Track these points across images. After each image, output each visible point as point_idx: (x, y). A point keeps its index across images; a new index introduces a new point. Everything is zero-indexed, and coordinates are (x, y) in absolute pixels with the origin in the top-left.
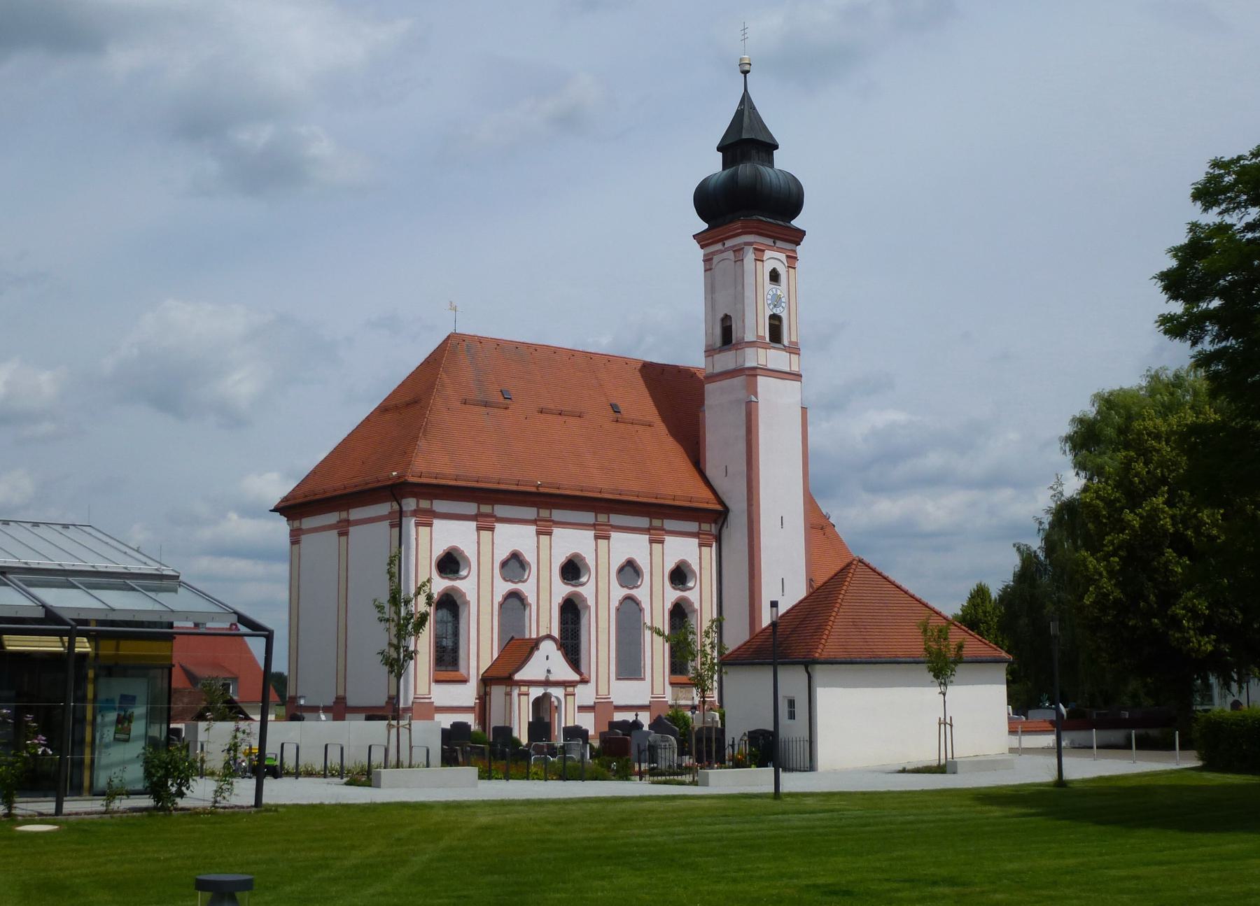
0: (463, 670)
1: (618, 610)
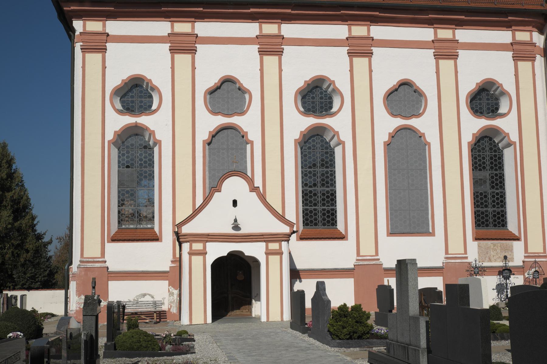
0: (340, 226)
1: (388, 145)
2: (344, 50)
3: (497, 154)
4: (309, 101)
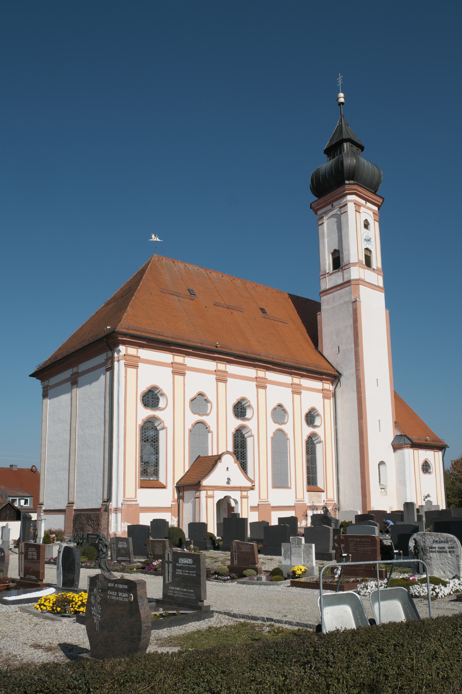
1: (272, 438)
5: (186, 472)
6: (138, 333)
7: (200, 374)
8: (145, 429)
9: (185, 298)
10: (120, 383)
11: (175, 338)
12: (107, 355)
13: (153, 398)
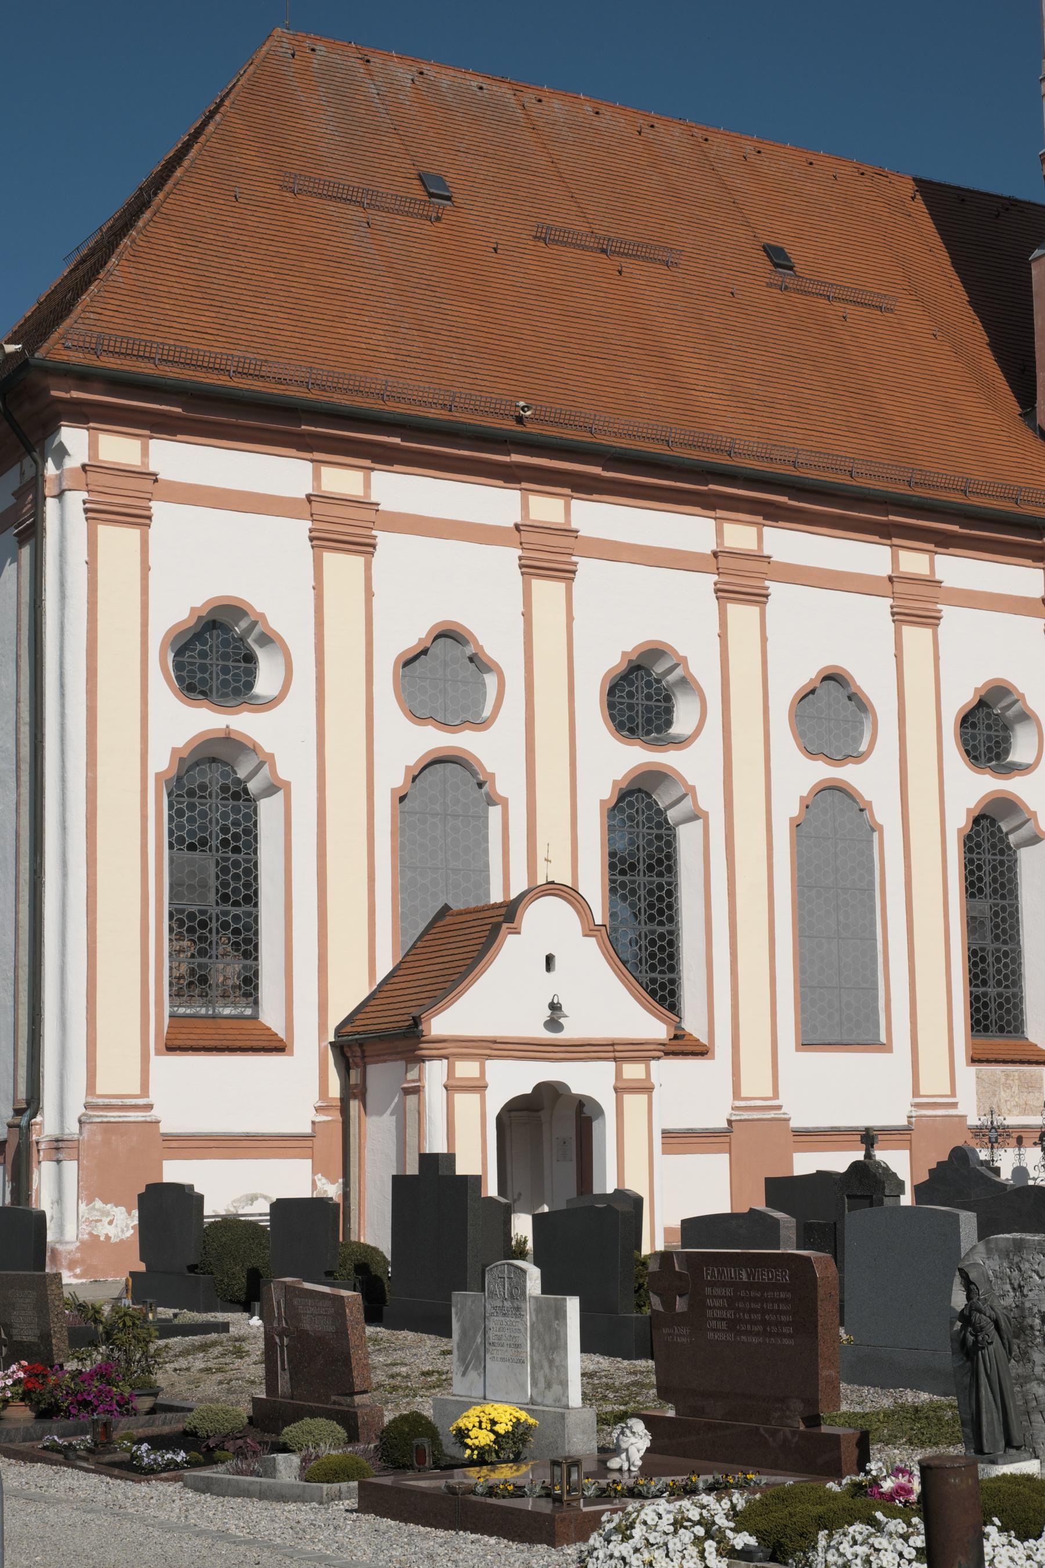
1: (797, 826)
2: (708, 581)
3: (1004, 858)
4: (622, 703)
5: (379, 978)
6: (145, 368)
7: (446, 549)
8: (191, 793)
9: (398, 212)
10: (69, 592)
11: (323, 388)
12: (22, 474)
13: (225, 657)
